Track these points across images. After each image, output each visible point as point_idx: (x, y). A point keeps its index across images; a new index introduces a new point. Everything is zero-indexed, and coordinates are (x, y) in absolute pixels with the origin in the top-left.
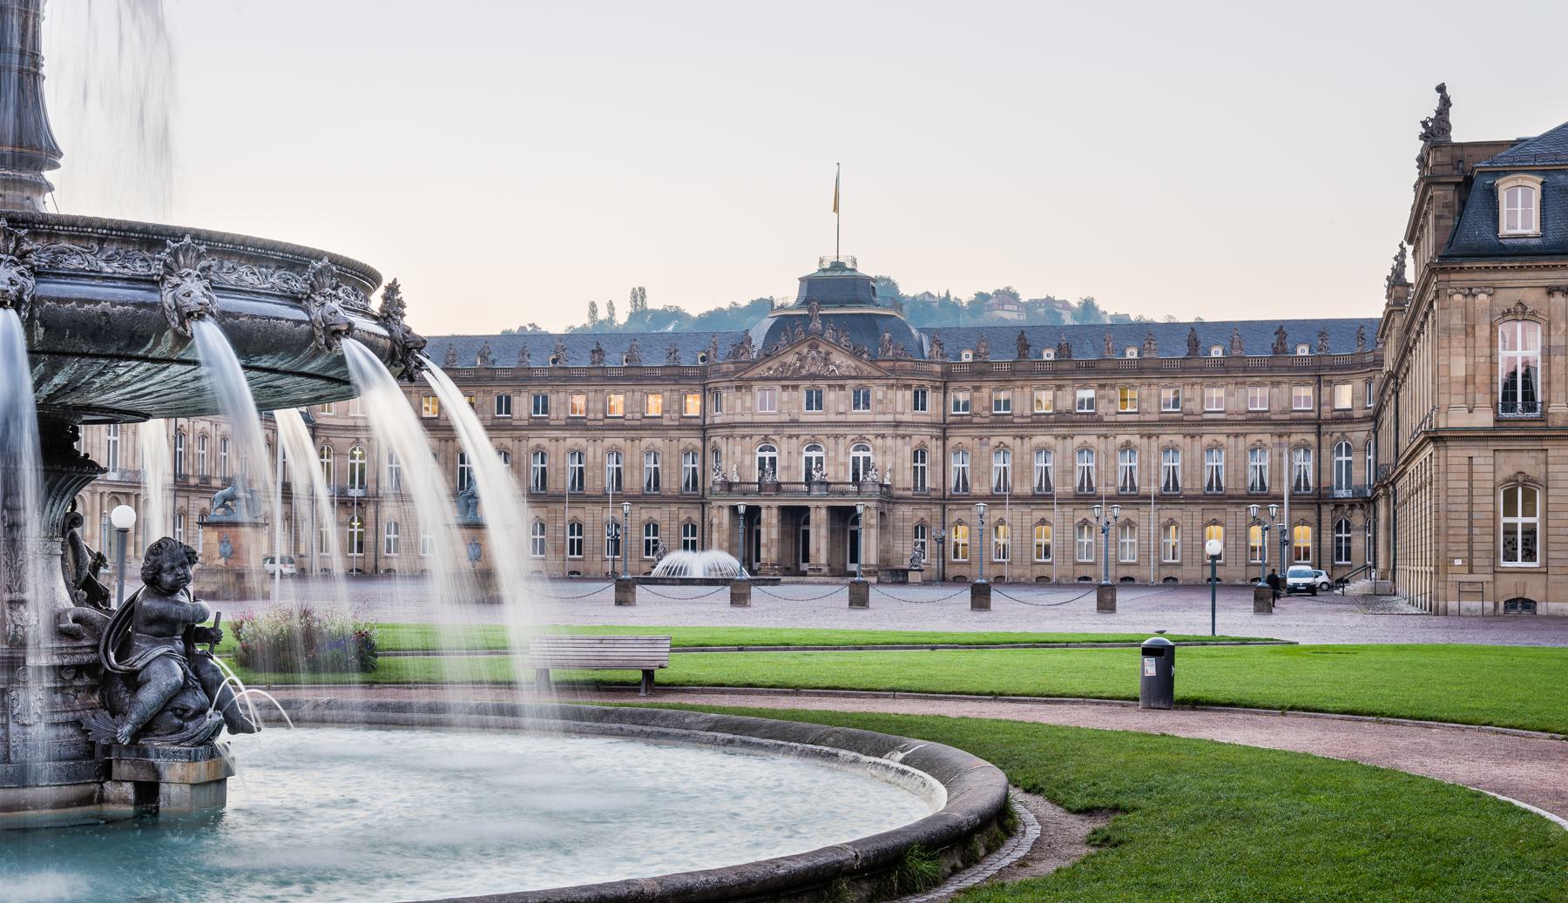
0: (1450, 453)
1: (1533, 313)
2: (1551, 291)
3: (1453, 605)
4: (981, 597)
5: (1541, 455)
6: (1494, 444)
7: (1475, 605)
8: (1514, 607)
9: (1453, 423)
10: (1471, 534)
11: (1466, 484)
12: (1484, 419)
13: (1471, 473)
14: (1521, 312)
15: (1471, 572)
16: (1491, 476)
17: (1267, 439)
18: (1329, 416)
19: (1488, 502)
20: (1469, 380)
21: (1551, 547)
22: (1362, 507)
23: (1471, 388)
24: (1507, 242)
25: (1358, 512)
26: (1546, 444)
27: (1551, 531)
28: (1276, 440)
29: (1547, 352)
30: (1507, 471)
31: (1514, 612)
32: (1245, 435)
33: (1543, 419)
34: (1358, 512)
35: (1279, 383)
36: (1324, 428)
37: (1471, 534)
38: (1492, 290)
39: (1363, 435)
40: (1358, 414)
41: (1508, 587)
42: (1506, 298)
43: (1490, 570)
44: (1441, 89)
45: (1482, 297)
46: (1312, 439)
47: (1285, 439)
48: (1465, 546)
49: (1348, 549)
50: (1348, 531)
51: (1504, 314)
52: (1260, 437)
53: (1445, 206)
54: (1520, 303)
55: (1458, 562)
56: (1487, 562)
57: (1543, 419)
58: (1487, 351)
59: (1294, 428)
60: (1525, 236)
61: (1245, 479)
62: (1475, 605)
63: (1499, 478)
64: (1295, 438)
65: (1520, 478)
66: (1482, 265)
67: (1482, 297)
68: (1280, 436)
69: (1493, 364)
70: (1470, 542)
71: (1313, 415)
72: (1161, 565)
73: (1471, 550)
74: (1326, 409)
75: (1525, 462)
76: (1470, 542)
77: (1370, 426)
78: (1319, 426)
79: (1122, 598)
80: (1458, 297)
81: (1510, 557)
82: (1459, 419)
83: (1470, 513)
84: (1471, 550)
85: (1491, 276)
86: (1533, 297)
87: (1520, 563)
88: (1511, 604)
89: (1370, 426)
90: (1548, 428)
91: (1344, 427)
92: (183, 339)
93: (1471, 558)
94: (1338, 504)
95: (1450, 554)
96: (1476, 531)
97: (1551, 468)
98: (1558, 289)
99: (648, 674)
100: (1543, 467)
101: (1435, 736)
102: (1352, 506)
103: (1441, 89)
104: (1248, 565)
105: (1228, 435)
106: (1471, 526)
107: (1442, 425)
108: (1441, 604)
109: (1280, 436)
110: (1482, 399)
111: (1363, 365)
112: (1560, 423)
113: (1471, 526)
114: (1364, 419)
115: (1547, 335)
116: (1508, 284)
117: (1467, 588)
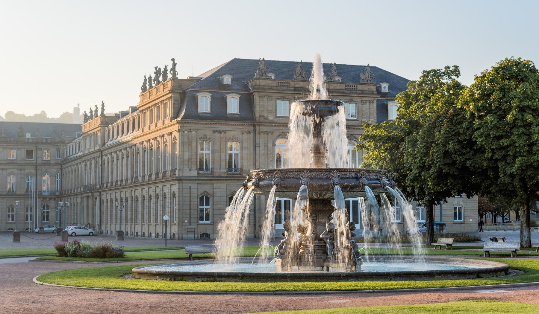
0: (184, 185)
1: (209, 139)
2: (214, 132)
3: (185, 236)
4: (17, 237)
5: (212, 186)
6: (197, 182)
7: (191, 236)
8: (203, 236)
9: (185, 174)
10: (190, 212)
11: (189, 195)
12: (194, 173)
13: (190, 191)
14: (205, 138)
15: (190, 225)
16: (196, 192)
17: (15, 171)
18: (41, 163)
19: (196, 201)
20: (190, 160)
21: (215, 216)
22: (55, 199)
23: (190, 163)
24: (200, 115)
25: (52, 201)
26: (213, 182)
27: (215, 211)
28: (19, 172)
29: (213, 152)
30: (201, 191)
31: (203, 238)
32: (6, 169)
33: (211, 173)
34: (52, 201)
35: (21, 148)
36: (38, 167)
37: (190, 212)
38: (197, 130)
39: (55, 171)
40: (53, 162)
41: (201, 230)
42: (201, 133)
43: (196, 224)
44: (173, 60)
45: (194, 132)
46: (33, 171)
47: (23, 171)
48: (188, 216)
49: (48, 216)
50: (48, 209)
51: (200, 139)
52: (12, 170)
53: (176, 100)
54: (205, 135)
55: (186, 221)
56: (195, 221)
57: (211, 173)
58: (195, 151)
59: (26, 167)
60: (206, 113)
61: (6, 187)
62: (191, 236)
63: (199, 193)
64: (27, 171)
65: (206, 193)
66: (194, 122)
67: (194, 132)
68: (21, 170)
69: (197, 155)
70: (190, 215)
71: (34, 162)
72: (7, 223)
73: (190, 217)
74: (39, 160)
75: (206, 188)
76: (190, 215)
77: (59, 167)
78: (36, 166)
79: (23, 239)
80: (186, 132)
81: (455, 219)
82: (187, 173)
83: (190, 205)
84: (190, 217)
85: (197, 126)
86: (209, 133)
87: (204, 222)
88: (202, 235)
89: (59, 167)
90: (213, 177)
91: (47, 167)
92: (363, 188)
93: (190, 220)
94: (44, 198)
95: (184, 219)
96: (192, 211)
97: (215, 190)
98: (217, 131)
99: (191, 255)
100: (212, 190)
101: (451, 256)
102: (50, 199)
103: (173, 60)
104: (7, 223)
105: (17, 169)
106: (190, 209)
107: (181, 175)
108: (180, 236)
109: (21, 170)
110: (194, 167)
111: (55, 143)
112: (217, 175)
113: (190, 209)
114: (56, 164)
115: (213, 146)
116: (202, 128)
117: (189, 230)
